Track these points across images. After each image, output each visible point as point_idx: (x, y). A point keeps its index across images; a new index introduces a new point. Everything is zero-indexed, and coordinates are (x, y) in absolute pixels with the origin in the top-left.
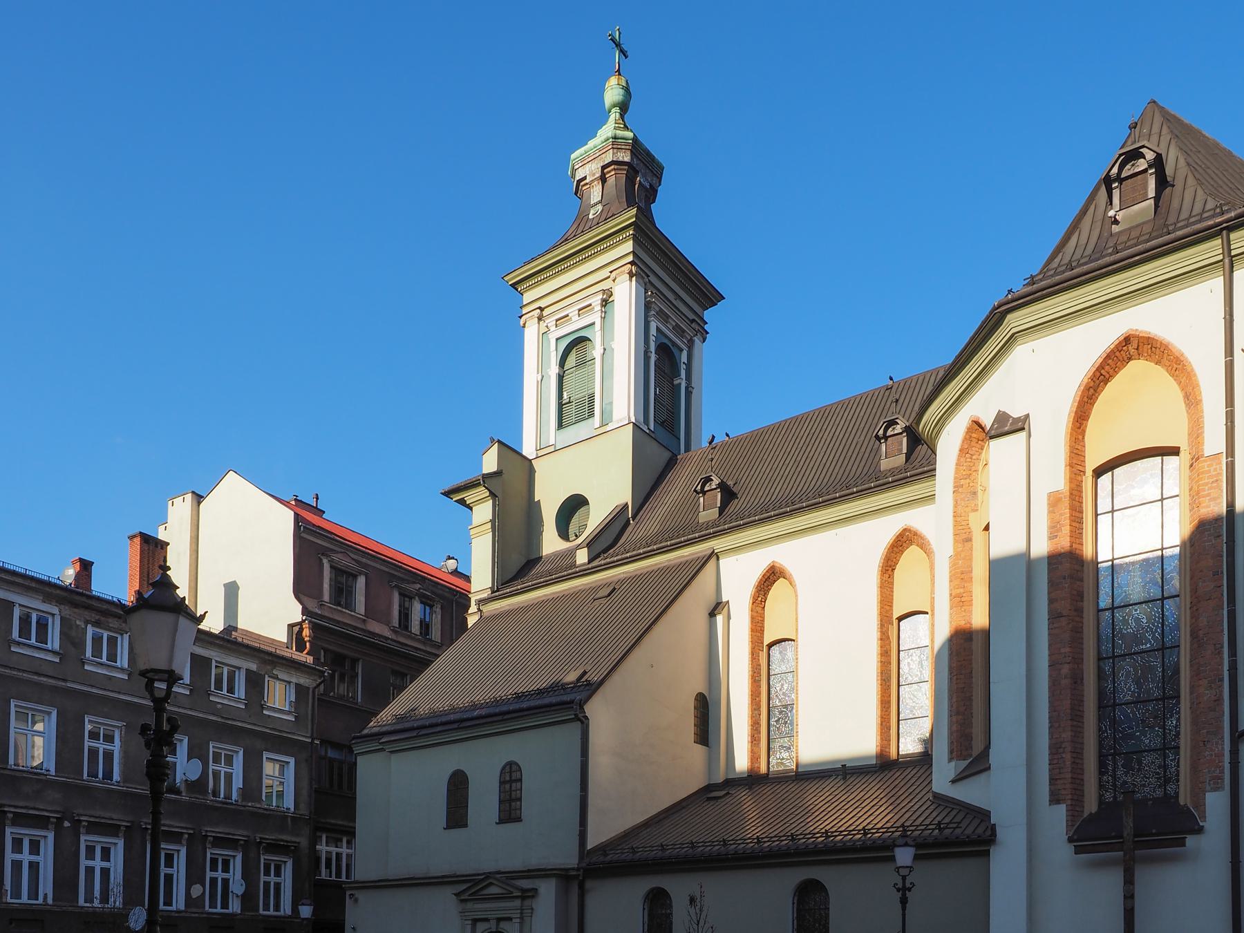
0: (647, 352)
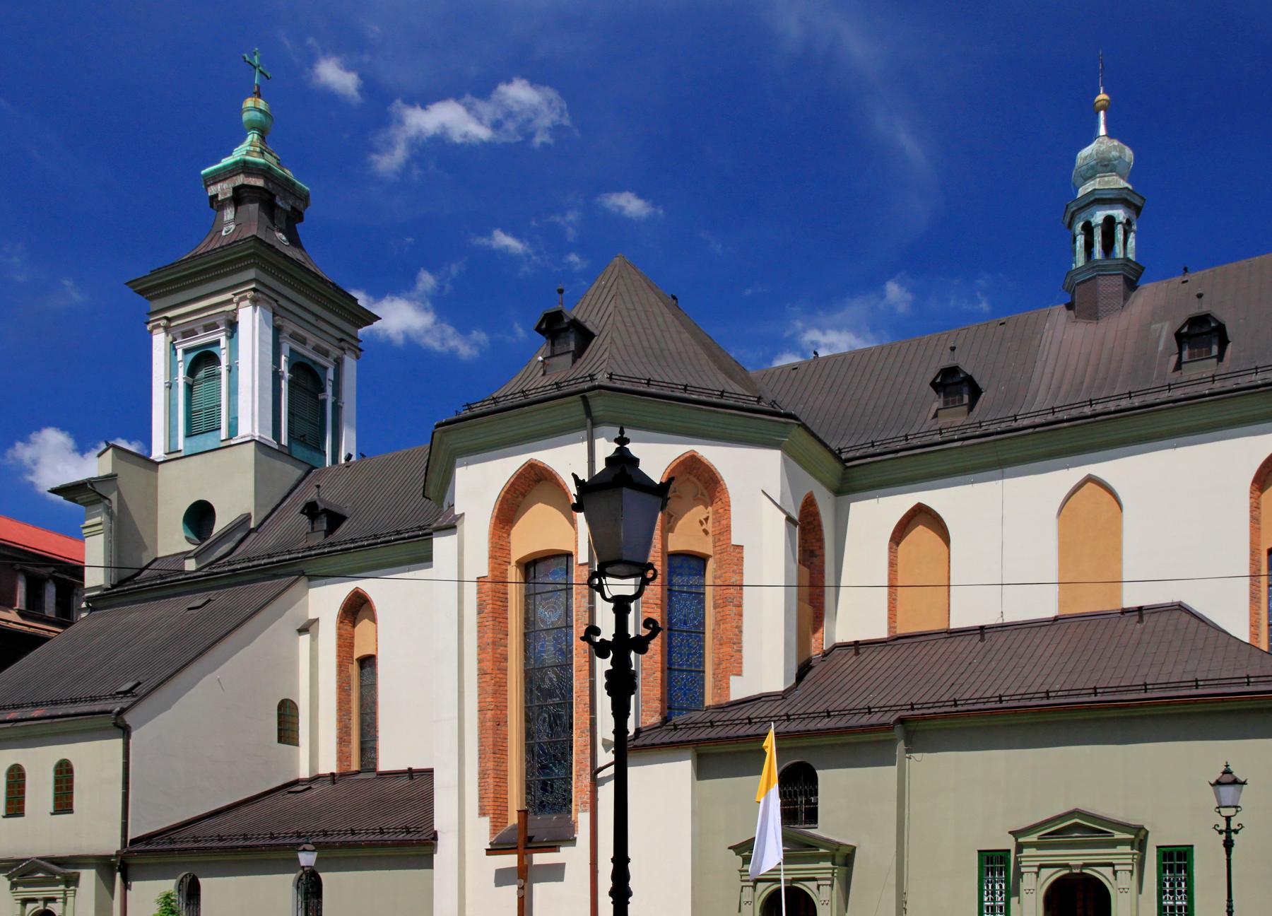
0: (277, 376)
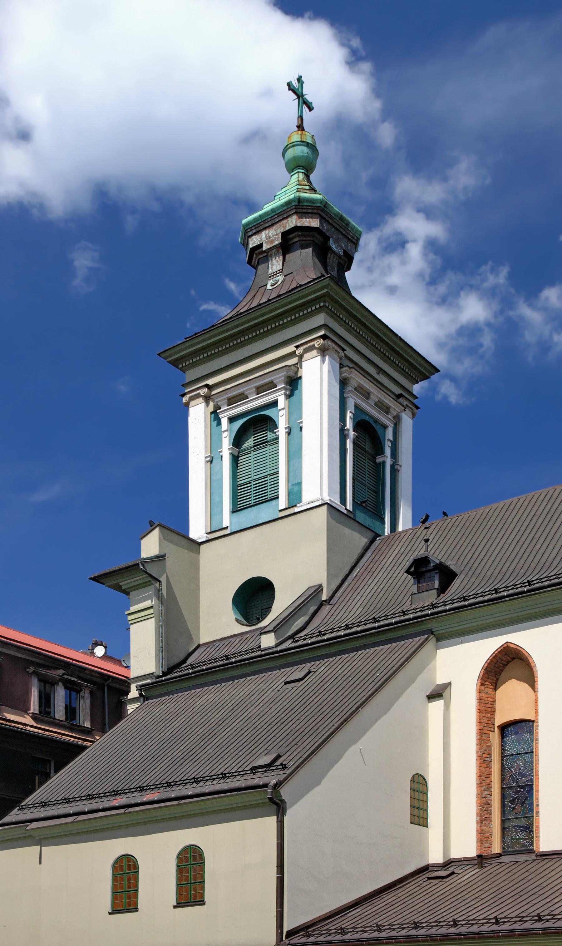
0: (343, 436)
